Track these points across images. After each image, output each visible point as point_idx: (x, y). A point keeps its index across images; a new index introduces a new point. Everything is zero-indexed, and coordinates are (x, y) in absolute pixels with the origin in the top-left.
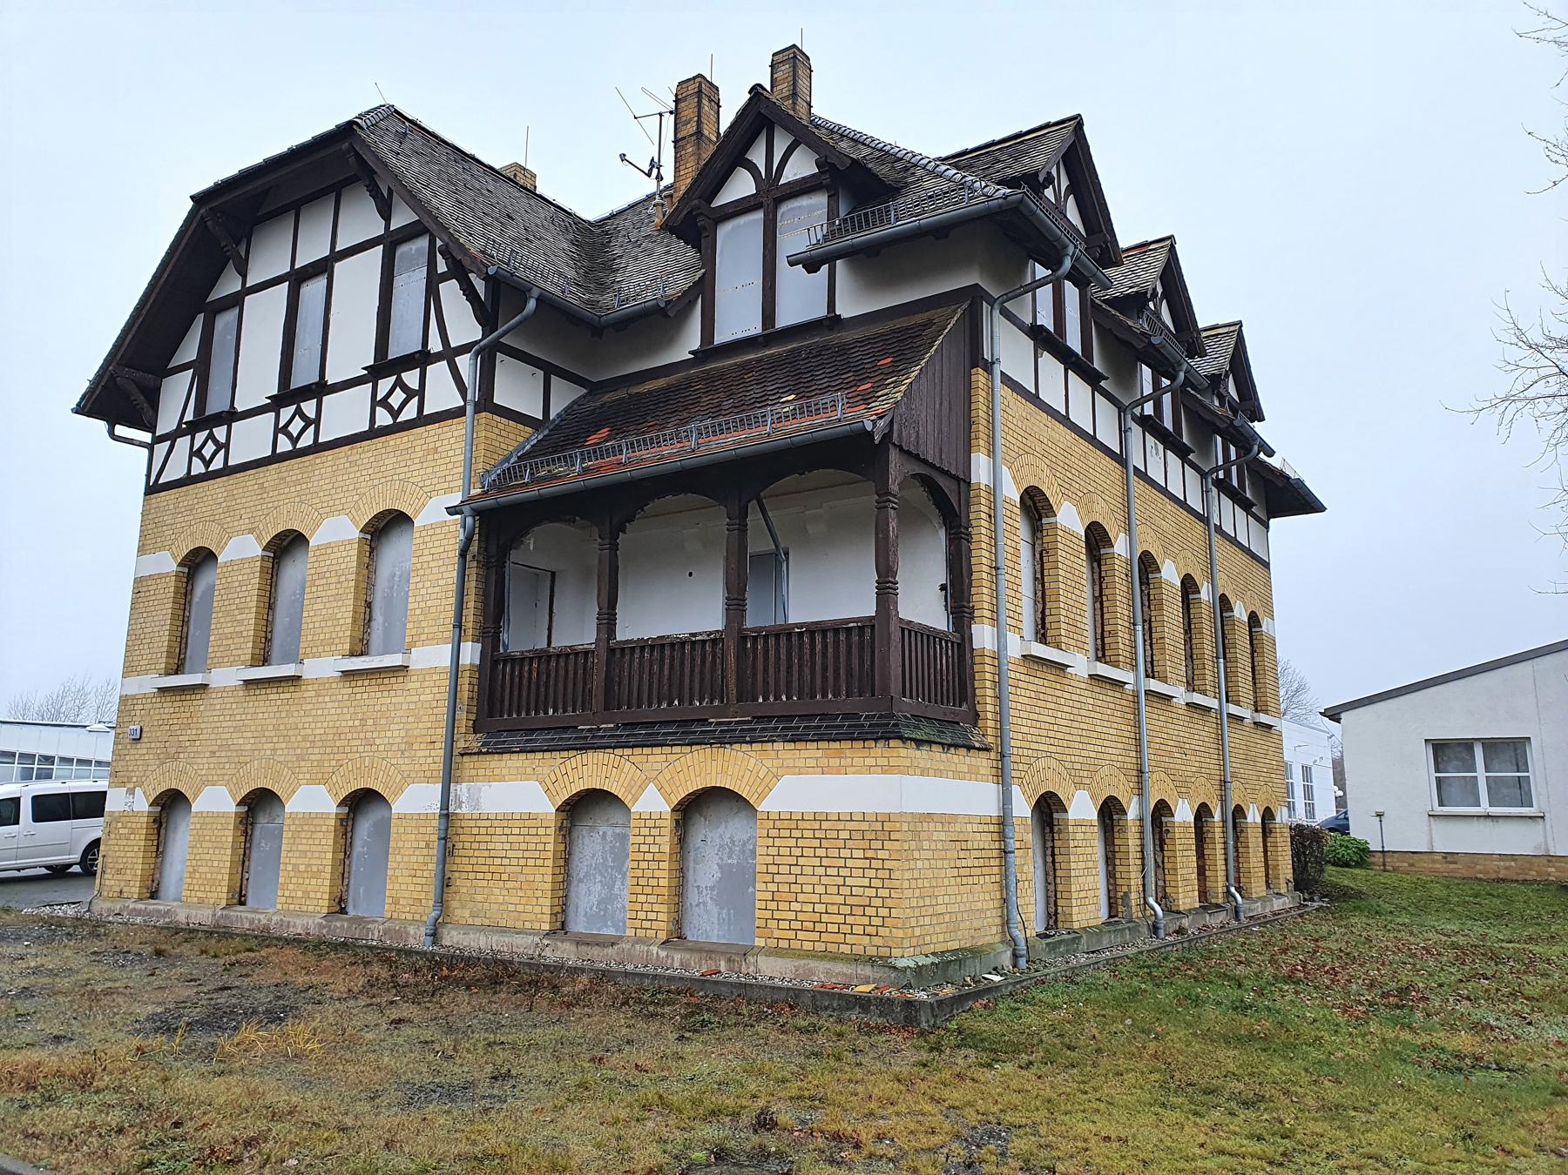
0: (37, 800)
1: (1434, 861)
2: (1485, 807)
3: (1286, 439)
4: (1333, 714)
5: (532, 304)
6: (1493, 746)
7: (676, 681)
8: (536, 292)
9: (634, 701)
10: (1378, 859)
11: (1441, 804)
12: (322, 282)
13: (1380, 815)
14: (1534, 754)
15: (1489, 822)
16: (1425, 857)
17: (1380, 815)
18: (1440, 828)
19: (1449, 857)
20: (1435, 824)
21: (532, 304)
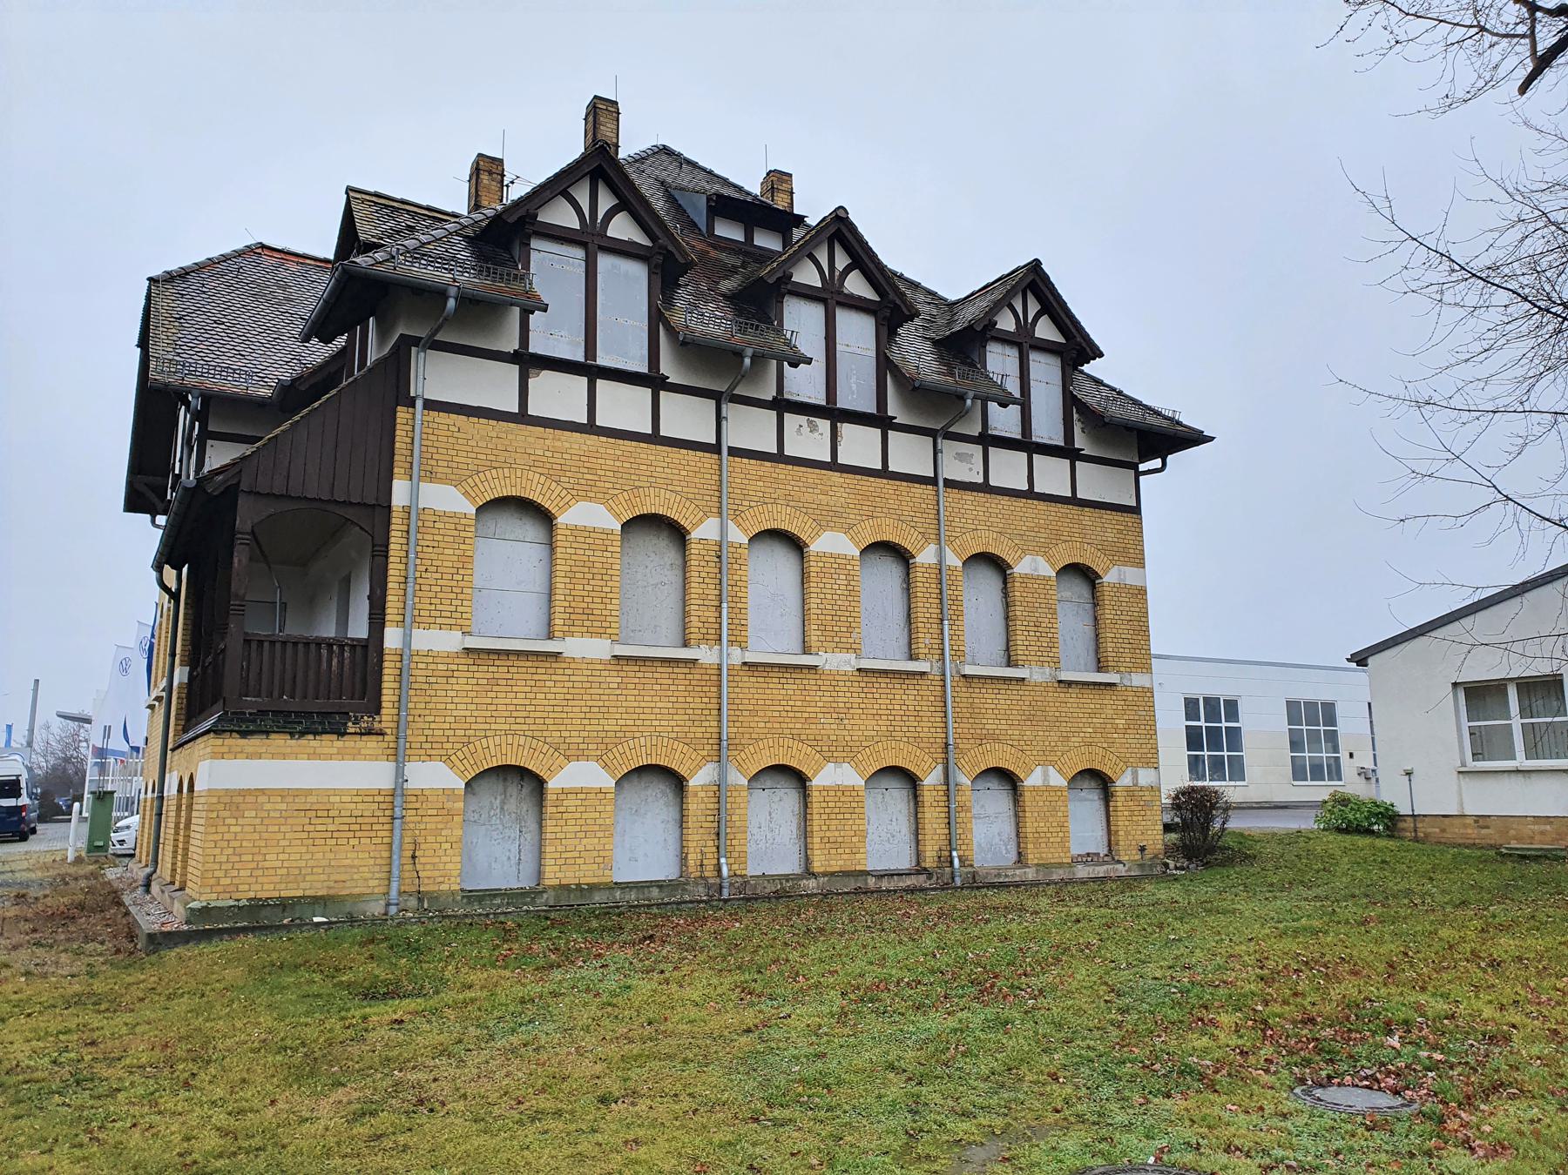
0: (18, 795)
1: (1465, 826)
2: (1521, 761)
3: (1129, 369)
4: (1360, 659)
5: (451, 303)
6: (1528, 687)
7: (288, 676)
8: (453, 291)
9: (311, 691)
10: (1409, 824)
11: (1476, 756)
12: (1541, 47)
13: (1409, 774)
14: (1294, 696)
15: (1520, 778)
16: (1457, 821)
17: (1409, 774)
18: (1471, 786)
19: (1481, 820)
20: (1466, 782)
21: (451, 303)
